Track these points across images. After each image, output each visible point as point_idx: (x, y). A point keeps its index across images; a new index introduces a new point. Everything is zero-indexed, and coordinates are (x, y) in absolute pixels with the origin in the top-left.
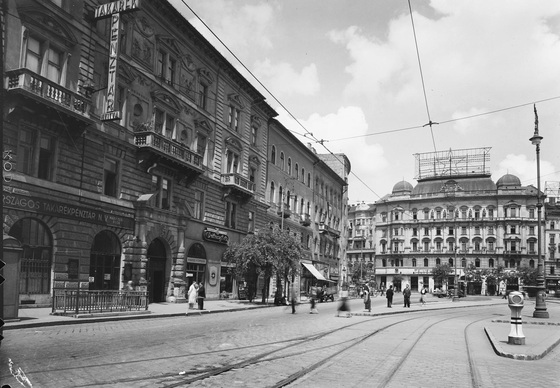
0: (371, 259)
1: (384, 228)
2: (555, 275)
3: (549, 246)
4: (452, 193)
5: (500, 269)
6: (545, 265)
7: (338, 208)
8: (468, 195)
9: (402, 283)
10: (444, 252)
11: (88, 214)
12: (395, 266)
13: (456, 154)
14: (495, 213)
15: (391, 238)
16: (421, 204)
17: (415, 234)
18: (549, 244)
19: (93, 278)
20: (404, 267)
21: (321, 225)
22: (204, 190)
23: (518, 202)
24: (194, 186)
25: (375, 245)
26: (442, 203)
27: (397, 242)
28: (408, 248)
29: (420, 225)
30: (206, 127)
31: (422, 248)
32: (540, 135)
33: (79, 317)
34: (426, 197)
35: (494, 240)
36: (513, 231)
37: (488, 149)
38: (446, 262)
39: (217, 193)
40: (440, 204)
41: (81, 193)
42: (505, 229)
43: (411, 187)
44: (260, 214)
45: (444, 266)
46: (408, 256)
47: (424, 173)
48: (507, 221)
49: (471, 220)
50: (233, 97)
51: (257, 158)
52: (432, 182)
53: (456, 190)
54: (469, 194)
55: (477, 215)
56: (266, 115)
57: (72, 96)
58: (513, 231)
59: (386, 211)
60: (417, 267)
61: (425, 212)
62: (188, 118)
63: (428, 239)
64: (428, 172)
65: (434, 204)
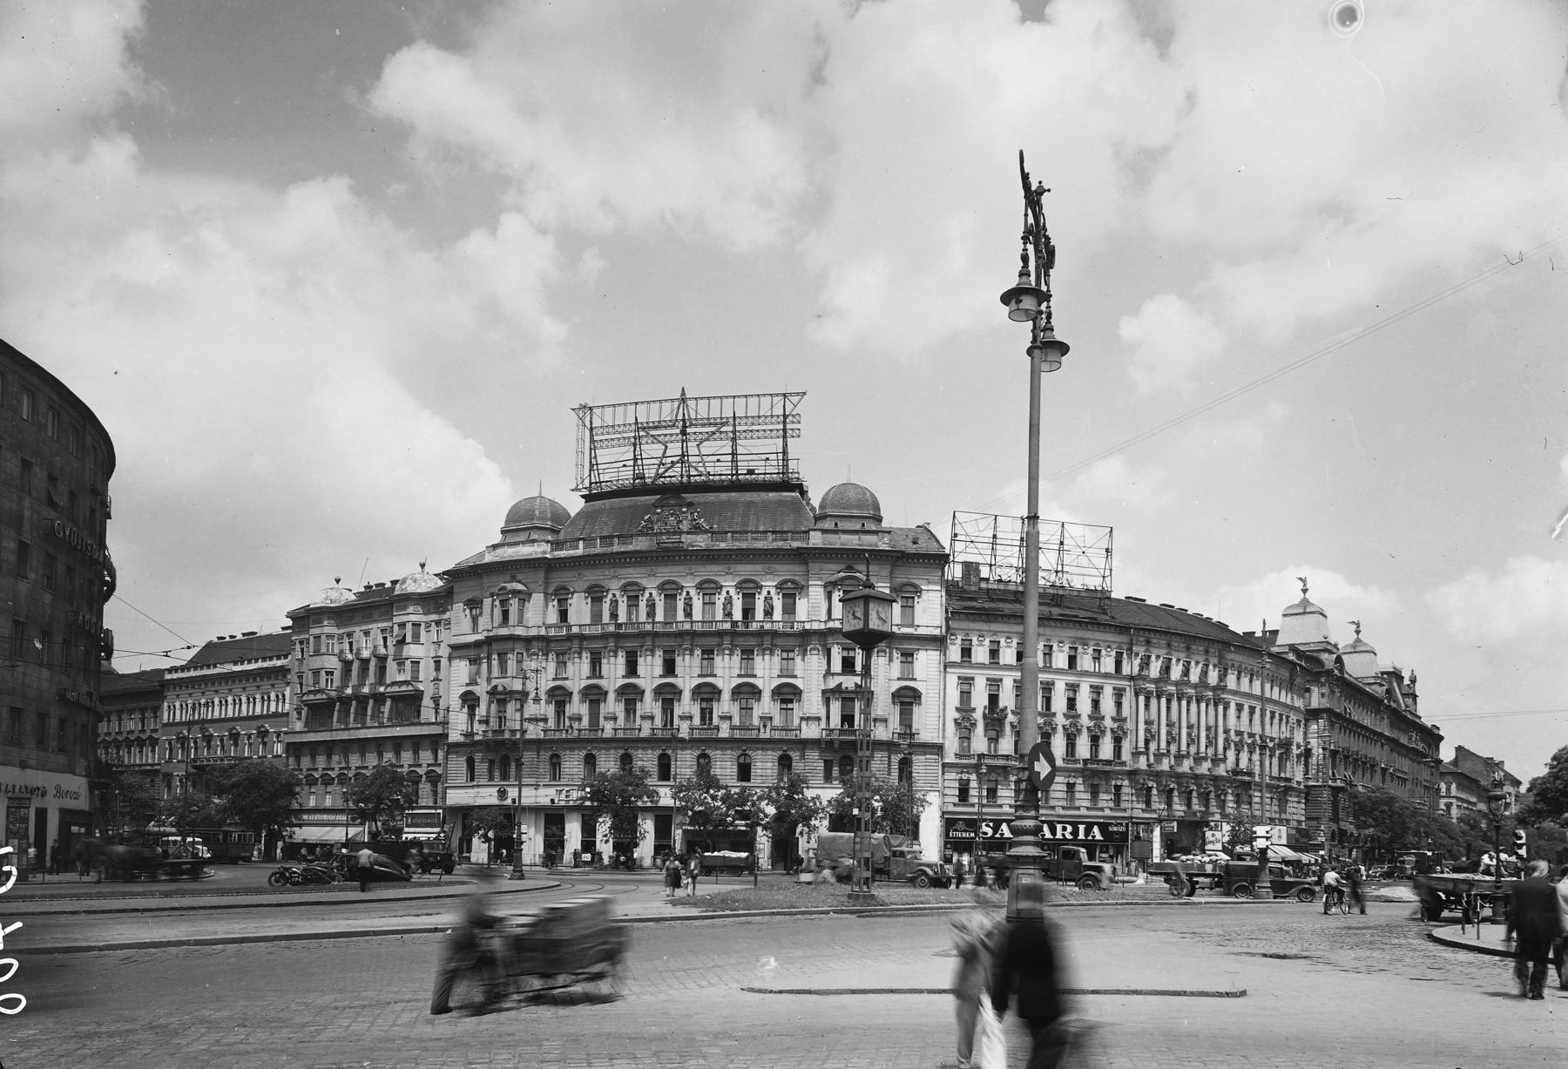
3: (957, 715)
6: (943, 773)
10: (645, 733)
12: (497, 781)
18: (957, 709)
36: (848, 666)
37: (795, 399)
40: (633, 574)
46: (538, 744)
48: (832, 632)
52: (626, 501)
53: (685, 526)
55: (748, 612)
59: (477, 594)
60: (563, 781)
64: (616, 467)
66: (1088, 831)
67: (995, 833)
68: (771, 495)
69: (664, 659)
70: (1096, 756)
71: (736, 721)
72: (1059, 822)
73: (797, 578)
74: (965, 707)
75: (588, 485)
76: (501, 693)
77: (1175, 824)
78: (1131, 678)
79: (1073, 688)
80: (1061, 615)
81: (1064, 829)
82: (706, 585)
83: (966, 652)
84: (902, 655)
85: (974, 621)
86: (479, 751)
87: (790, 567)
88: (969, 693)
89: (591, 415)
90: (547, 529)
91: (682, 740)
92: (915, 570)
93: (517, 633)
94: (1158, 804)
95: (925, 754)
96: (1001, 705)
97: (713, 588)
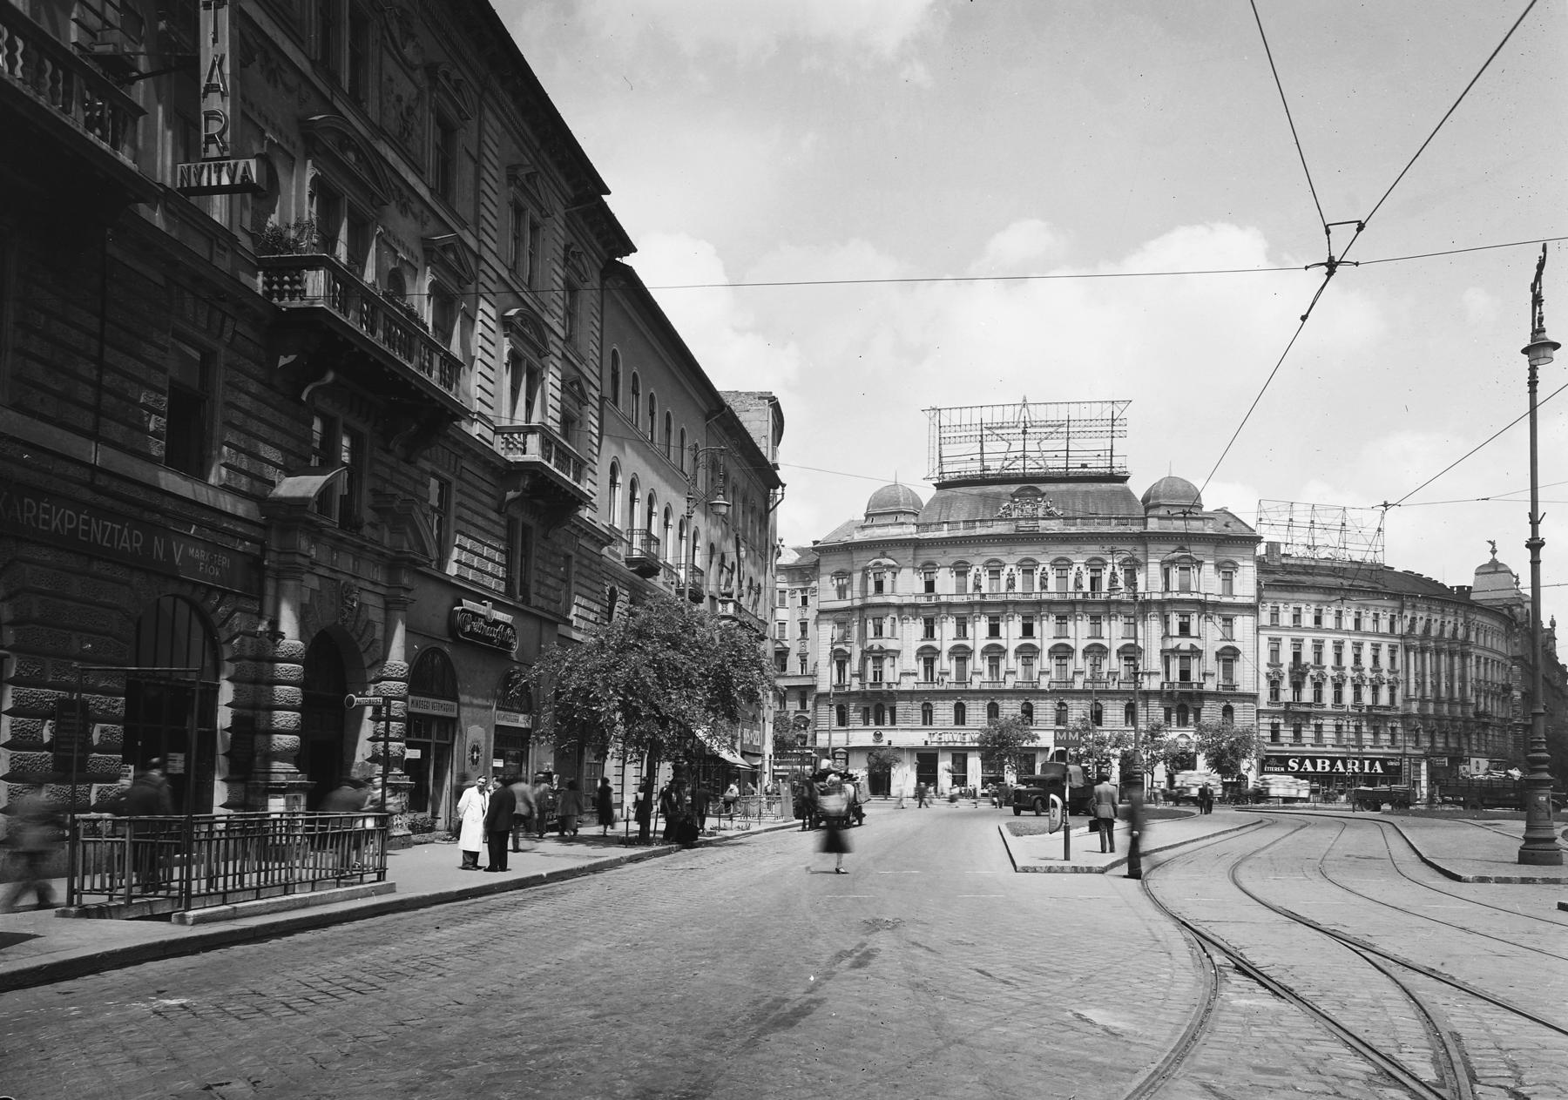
0: (803, 705)
1: (841, 617)
2: (1282, 745)
3: (1268, 670)
4: (1031, 523)
5: (1155, 731)
7: (758, 553)
8: (1073, 530)
9: (893, 771)
10: (1009, 686)
11: (121, 532)
12: (872, 725)
13: (1038, 414)
15: (862, 645)
16: (948, 550)
17: (929, 633)
18: (1269, 665)
19: (132, 767)
20: (898, 726)
21: (724, 602)
22: (453, 474)
23: (1196, 551)
24: (426, 459)
25: (816, 665)
26: (1005, 549)
27: (880, 656)
28: (909, 674)
29: (944, 611)
30: (455, 266)
31: (947, 674)
32: (1551, 336)
33: (200, 920)
34: (961, 532)
36: (1184, 630)
37: (1122, 406)
38: (1014, 711)
39: (485, 487)
41: (95, 454)
42: (1166, 623)
43: (917, 502)
44: (586, 562)
45: (1009, 726)
46: (910, 695)
47: (953, 463)
48: (1171, 602)
49: (1080, 596)
50: (522, 173)
51: (579, 384)
52: (976, 490)
53: (1041, 513)
54: (1075, 525)
56: (599, 247)
57: (75, 77)
58: (1184, 630)
59: (846, 567)
60: (934, 726)
61: (958, 574)
62: (405, 228)
63: (965, 647)
65: (982, 550)
66: (1372, 766)
67: (1300, 767)
68: (1103, 485)
71: (1088, 676)
74: (1275, 663)
76: (876, 652)
78: (1402, 637)
79: (1358, 646)
81: (1354, 764)
82: (1059, 563)
83: (1275, 614)
84: (1224, 620)
86: (854, 701)
88: (1277, 651)
91: (1044, 692)
92: (1233, 550)
93: (891, 601)
94: (1426, 742)
95: (1244, 702)
96: (1304, 660)
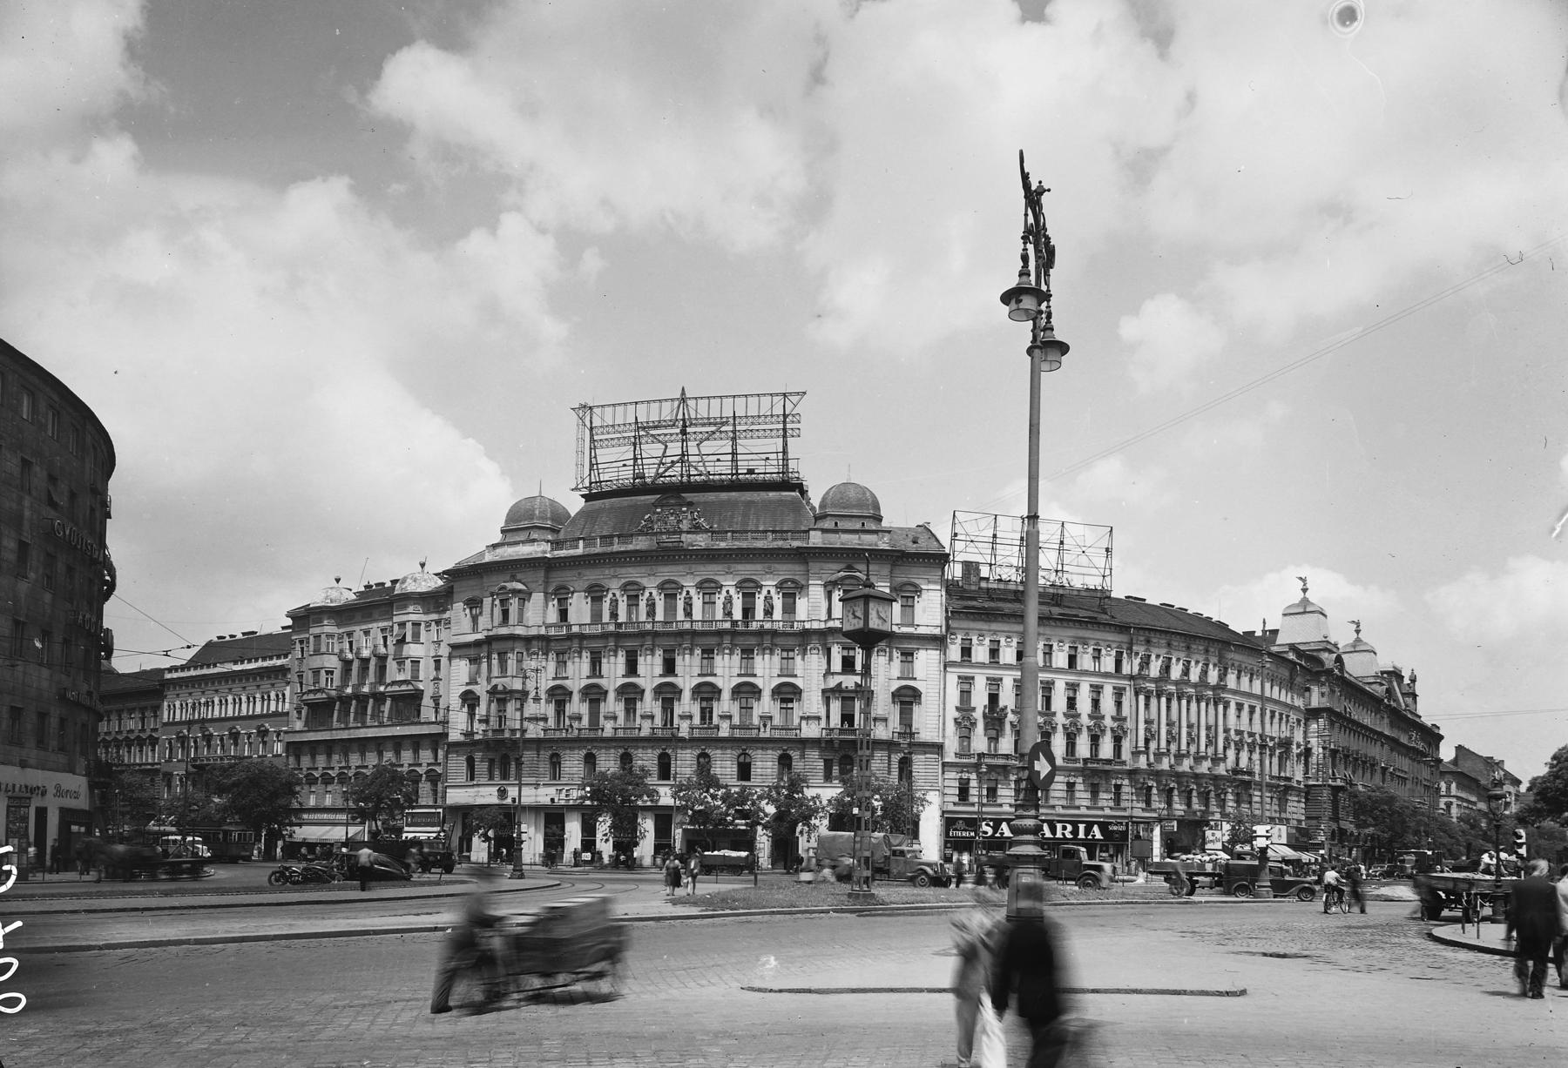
3: (957, 715)
10: (645, 732)
12: (497, 780)
14: (802, 605)
18: (957, 708)
35: (795, 693)
36: (848, 665)
37: (795, 399)
40: (633, 573)
46: (538, 743)
48: (832, 631)
52: (626, 500)
53: (685, 526)
55: (748, 611)
59: (477, 593)
60: (563, 781)
64: (616, 466)
66: (1088, 830)
67: (995, 832)
68: (771, 494)
69: (664, 658)
70: (1096, 755)
72: (1059, 822)
73: (797, 578)
74: (965, 707)
75: (588, 485)
76: (501, 693)
77: (1175, 823)
78: (1131, 677)
79: (1073, 687)
80: (1061, 614)
81: (1064, 828)
82: (706, 585)
83: (966, 652)
84: (902, 654)
85: (974, 620)
87: (790, 566)
88: (969, 692)
89: (591, 415)
90: (547, 528)
91: (682, 740)
92: (915, 570)
93: (517, 632)
94: (1158, 803)
95: (925, 753)
96: (1001, 704)
97: (713, 588)
